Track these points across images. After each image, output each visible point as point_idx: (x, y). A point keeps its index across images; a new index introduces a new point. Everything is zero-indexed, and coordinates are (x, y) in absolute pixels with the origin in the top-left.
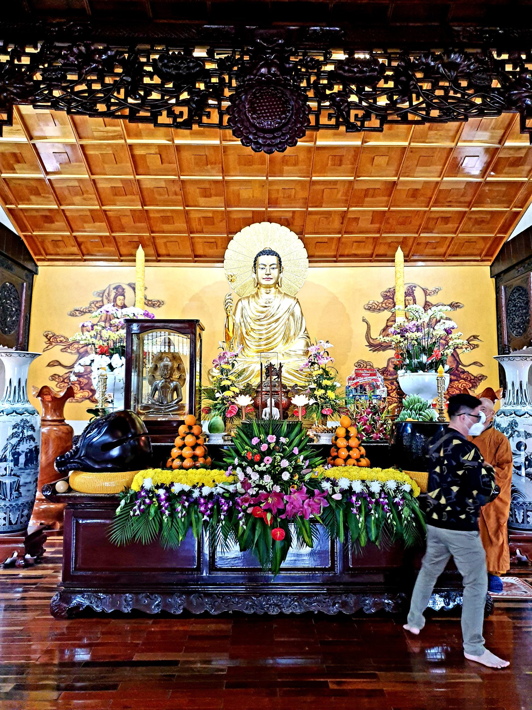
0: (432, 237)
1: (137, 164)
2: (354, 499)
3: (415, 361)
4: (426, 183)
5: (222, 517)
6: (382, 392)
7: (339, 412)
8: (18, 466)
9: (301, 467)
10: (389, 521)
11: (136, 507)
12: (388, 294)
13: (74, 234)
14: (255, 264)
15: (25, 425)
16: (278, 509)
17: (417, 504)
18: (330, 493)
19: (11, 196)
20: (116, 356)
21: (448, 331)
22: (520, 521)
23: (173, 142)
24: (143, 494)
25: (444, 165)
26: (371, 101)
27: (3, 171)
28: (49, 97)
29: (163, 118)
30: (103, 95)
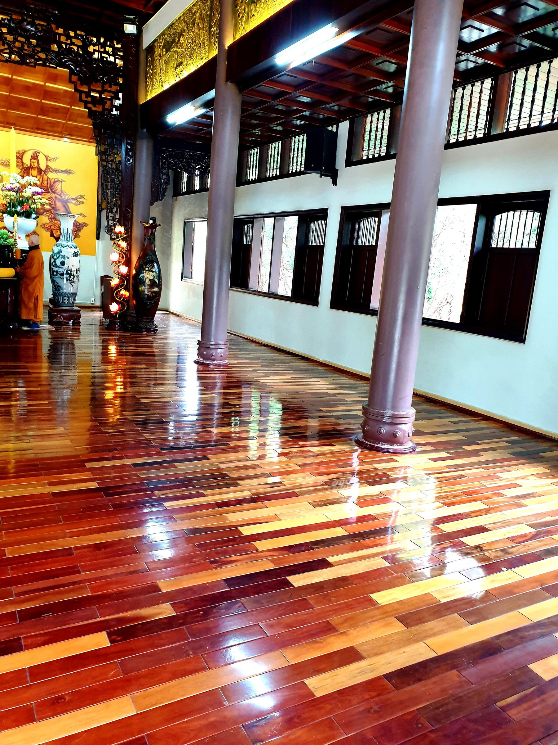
22: (61, 302)
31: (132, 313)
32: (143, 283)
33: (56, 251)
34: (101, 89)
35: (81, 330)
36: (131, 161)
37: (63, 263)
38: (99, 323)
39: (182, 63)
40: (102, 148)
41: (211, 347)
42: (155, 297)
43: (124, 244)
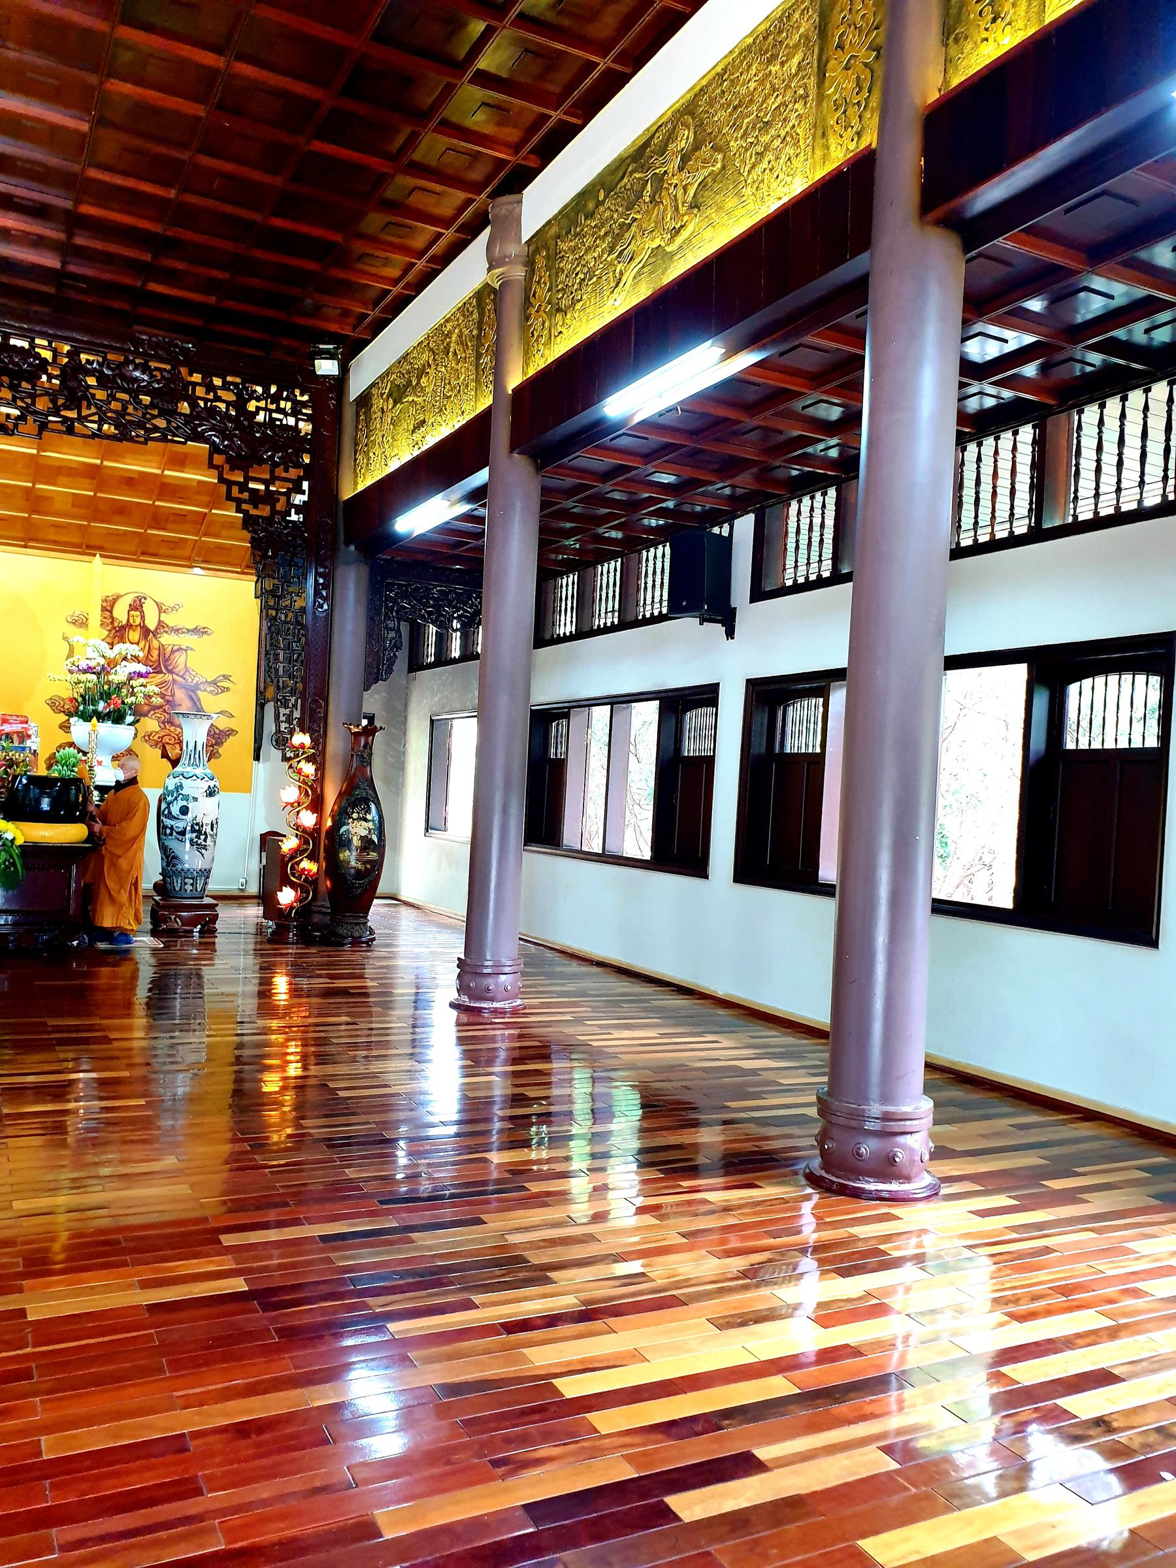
26: (29, 401)
31: (323, 906)
32: (347, 844)
33: (171, 787)
34: (267, 476)
35: (217, 947)
36: (325, 607)
37: (184, 811)
38: (253, 930)
39: (424, 422)
40: (269, 584)
41: (486, 971)
42: (371, 873)
43: (309, 769)
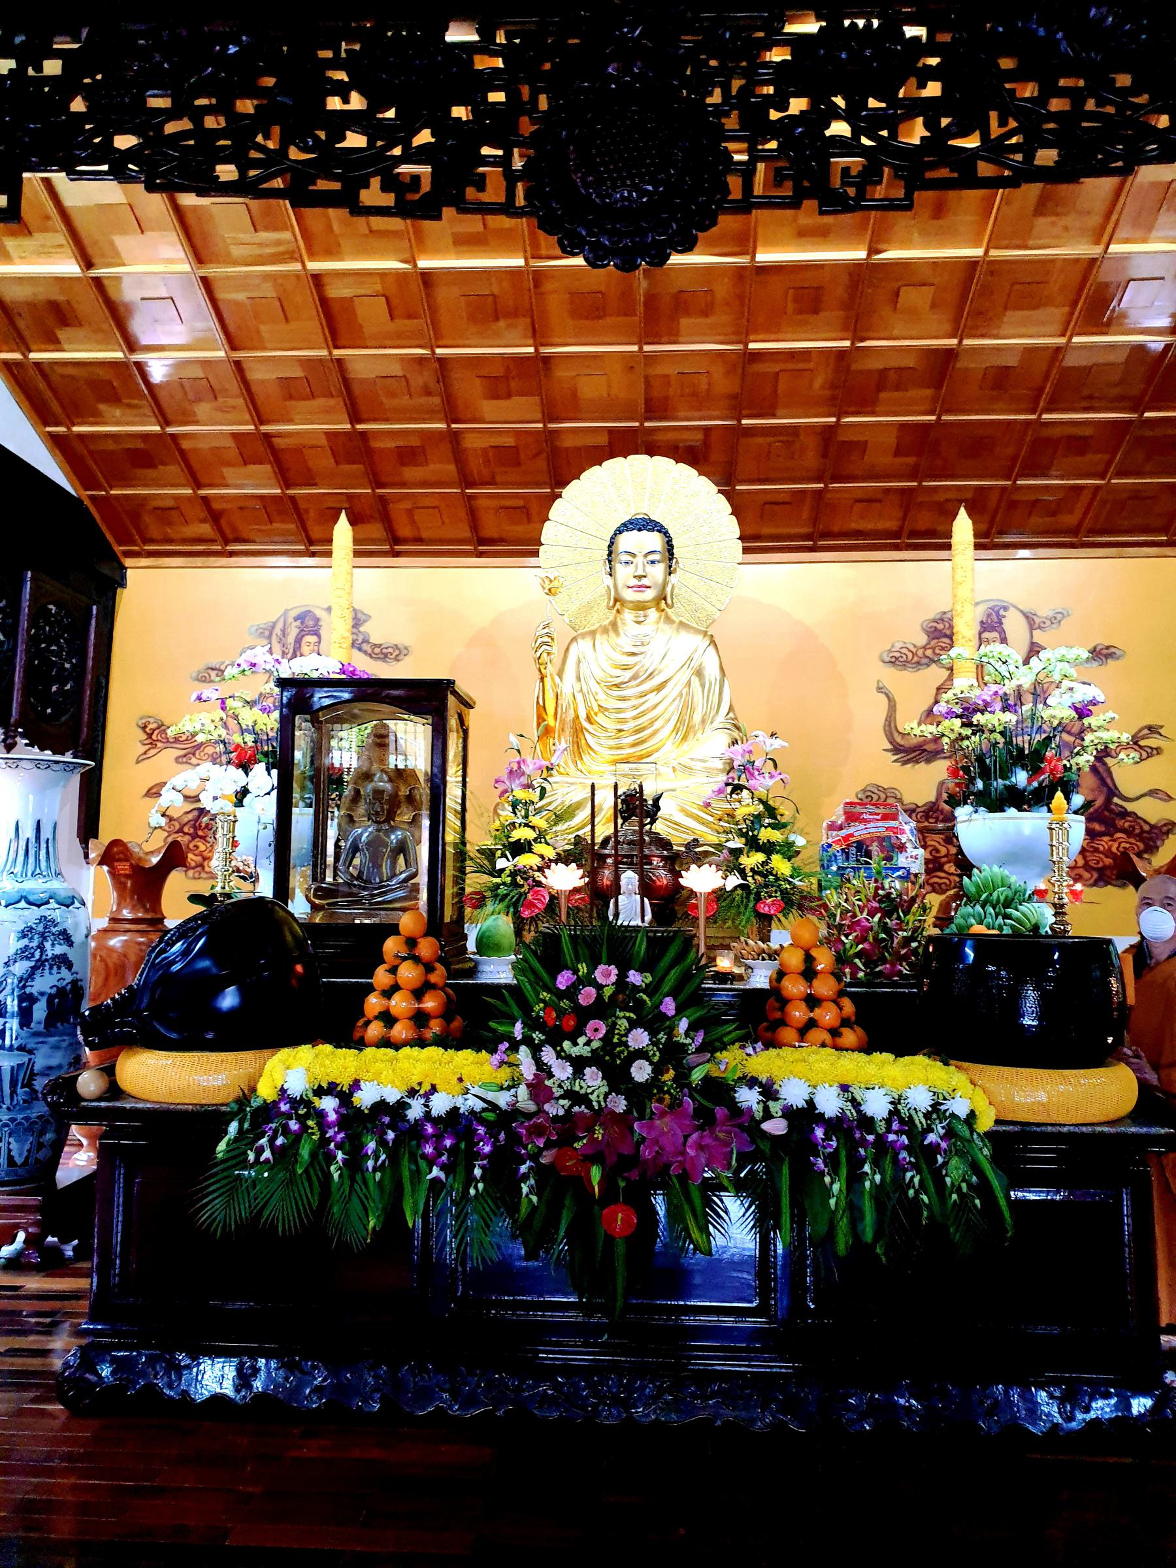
0: (1047, 487)
1: (336, 321)
2: (819, 1133)
3: (999, 784)
4: (1029, 350)
5: (478, 1172)
6: (913, 859)
7: (801, 907)
8: (28, 1026)
9: (683, 1047)
10: (911, 1192)
11: (264, 1141)
12: (940, 626)
13: (202, 492)
14: (610, 554)
15: (46, 930)
16: (620, 1156)
17: (986, 1152)
18: (759, 1115)
19: (55, 406)
20: (259, 769)
21: (1082, 712)
23: (415, 266)
24: (284, 1107)
25: (1074, 304)
27: (33, 347)
28: (106, 153)
29: (373, 195)
30: (229, 143)
